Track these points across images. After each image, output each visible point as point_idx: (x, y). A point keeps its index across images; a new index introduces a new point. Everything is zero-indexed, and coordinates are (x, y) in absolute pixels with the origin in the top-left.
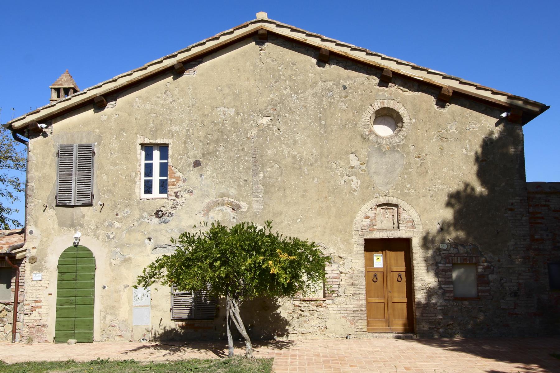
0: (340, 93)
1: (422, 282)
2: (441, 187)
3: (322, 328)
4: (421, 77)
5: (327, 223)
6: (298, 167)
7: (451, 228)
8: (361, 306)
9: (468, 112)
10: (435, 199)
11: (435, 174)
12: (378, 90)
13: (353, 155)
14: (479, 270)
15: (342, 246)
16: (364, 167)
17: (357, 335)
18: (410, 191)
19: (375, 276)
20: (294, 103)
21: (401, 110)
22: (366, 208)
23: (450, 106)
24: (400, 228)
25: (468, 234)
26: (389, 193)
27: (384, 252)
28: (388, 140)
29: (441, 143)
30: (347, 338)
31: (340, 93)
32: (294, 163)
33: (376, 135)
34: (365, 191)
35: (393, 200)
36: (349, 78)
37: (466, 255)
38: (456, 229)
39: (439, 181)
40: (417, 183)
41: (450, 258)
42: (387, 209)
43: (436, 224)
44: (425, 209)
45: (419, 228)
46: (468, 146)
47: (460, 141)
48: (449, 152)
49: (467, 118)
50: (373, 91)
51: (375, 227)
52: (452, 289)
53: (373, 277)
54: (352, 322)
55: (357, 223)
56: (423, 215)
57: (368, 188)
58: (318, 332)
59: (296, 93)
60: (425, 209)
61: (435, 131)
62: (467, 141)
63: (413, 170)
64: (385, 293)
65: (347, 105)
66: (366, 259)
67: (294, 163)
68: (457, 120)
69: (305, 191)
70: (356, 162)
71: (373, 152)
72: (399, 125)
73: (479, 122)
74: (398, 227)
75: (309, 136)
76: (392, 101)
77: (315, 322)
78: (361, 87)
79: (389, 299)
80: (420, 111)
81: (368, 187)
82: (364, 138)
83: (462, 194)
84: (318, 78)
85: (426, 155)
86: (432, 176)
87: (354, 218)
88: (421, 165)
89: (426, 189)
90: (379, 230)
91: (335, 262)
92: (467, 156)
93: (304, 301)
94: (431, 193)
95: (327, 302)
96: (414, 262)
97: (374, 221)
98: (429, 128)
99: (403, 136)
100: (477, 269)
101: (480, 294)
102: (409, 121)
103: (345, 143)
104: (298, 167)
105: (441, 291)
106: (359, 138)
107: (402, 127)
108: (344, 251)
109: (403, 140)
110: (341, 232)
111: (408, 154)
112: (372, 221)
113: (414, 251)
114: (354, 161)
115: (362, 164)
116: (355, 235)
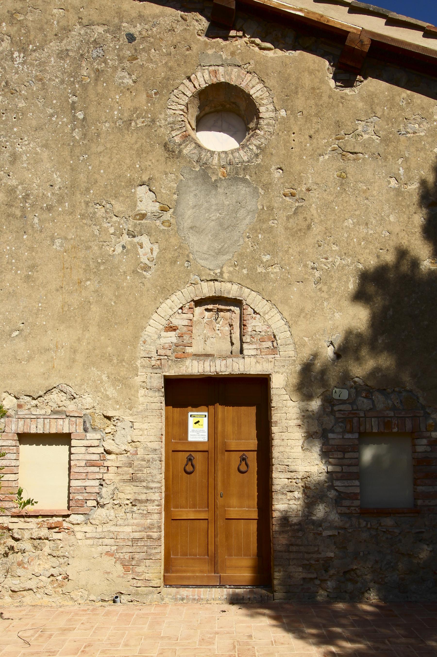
0: (120, 49)
1: (289, 475)
2: (338, 261)
3: (60, 578)
4: (301, 10)
5: (79, 340)
6: (18, 213)
7: (364, 352)
8: (150, 528)
9: (404, 95)
10: (325, 288)
11: (327, 232)
12: (206, 44)
13: (144, 188)
14: (420, 449)
15: (111, 392)
16: (167, 216)
17: (137, 594)
18: (270, 269)
19: (190, 460)
20: (17, 73)
21: (256, 91)
22: (169, 306)
23: (365, 82)
24: (245, 352)
25: (401, 364)
26: (222, 273)
27: (211, 407)
28: (223, 156)
29: (341, 164)
30: (114, 602)
31: (120, 49)
32: (9, 205)
33: (199, 146)
34: (168, 269)
35: (231, 290)
36: (141, 17)
37: (391, 414)
38: (374, 349)
39: (335, 248)
40: (287, 252)
41: (355, 420)
42: (222, 310)
43: (326, 344)
44: (302, 310)
45: (288, 351)
46: (402, 171)
47: (386, 159)
48: (360, 185)
49: (403, 109)
50: (195, 47)
51: (189, 350)
52: (358, 490)
53: (182, 460)
54: (128, 565)
55: (149, 340)
56: (296, 322)
57: (175, 262)
58: (50, 587)
59: (23, 50)
60: (302, 310)
61: (330, 136)
62: (400, 161)
63: (278, 225)
64: (210, 499)
65: (134, 77)
66: (169, 422)
67: (9, 205)
68: (379, 114)
69: (33, 267)
70: (151, 204)
71: (190, 183)
72: (252, 125)
73: (426, 117)
74: (241, 352)
75: (46, 146)
76: (236, 70)
77: (42, 565)
78: (169, 38)
79: (218, 512)
80: (296, 93)
81: (177, 257)
82: (171, 152)
83: (391, 275)
84: (73, 17)
85: (308, 190)
86: (319, 238)
87: (143, 328)
88: (295, 213)
89: (305, 266)
90: (197, 356)
91: (94, 429)
92: (398, 192)
93: (19, 516)
94: (317, 274)
95: (73, 518)
96: (274, 429)
97: (186, 337)
98: (317, 131)
99: (258, 147)
100: (414, 445)
101: (419, 502)
102: (272, 115)
103: (128, 161)
104: (18, 213)
105: (332, 494)
106: (159, 150)
107: (257, 128)
108: (117, 402)
109: (257, 155)
110: (111, 361)
111: (267, 187)
112: (184, 335)
113: (273, 404)
114: (146, 202)
115: (163, 210)
116: (144, 367)
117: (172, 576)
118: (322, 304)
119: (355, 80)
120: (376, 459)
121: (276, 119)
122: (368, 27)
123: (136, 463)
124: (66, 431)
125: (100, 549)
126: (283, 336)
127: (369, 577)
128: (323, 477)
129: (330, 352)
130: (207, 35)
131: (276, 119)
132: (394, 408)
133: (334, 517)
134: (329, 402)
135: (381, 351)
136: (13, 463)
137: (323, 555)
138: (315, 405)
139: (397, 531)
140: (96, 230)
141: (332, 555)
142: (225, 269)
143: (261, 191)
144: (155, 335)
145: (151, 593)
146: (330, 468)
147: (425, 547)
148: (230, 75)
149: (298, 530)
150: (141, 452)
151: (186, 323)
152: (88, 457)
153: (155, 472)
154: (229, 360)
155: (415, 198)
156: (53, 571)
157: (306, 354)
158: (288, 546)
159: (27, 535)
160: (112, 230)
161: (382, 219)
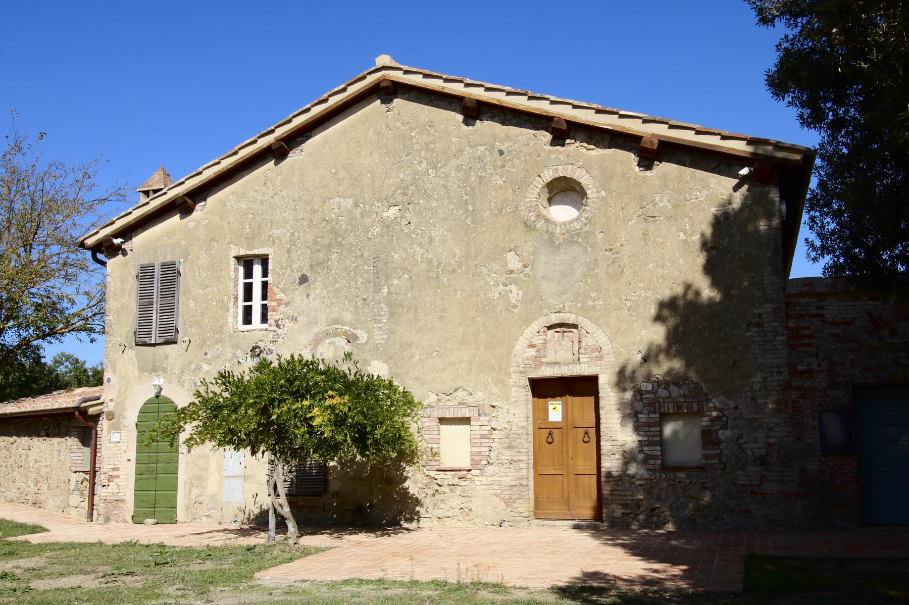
0: (495, 161)
5: (474, 356)
6: (434, 276)
7: (662, 357)
8: (521, 478)
10: (634, 314)
12: (550, 151)
15: (495, 390)
17: (514, 521)
18: (596, 302)
25: (688, 365)
26: (564, 307)
31: (495, 161)
33: (547, 221)
35: (571, 318)
39: (641, 285)
40: (608, 290)
41: (657, 404)
43: (636, 353)
44: (619, 329)
46: (688, 227)
47: (676, 219)
48: (658, 239)
49: (687, 182)
50: (542, 154)
51: (544, 360)
53: (546, 434)
54: (508, 502)
60: (619, 329)
65: (504, 179)
69: (444, 310)
73: (706, 186)
75: (450, 230)
76: (570, 167)
77: (455, 502)
80: (612, 179)
82: (529, 227)
83: (681, 302)
85: (622, 245)
87: (514, 347)
88: (613, 262)
89: (621, 299)
92: (685, 242)
94: (629, 304)
97: (542, 352)
98: (627, 204)
99: (586, 219)
102: (596, 195)
104: (434, 276)
105: (641, 456)
106: (521, 226)
108: (498, 396)
109: (586, 224)
114: (513, 262)
115: (525, 266)
117: (540, 511)
118: (633, 325)
119: (653, 164)
120: (675, 433)
121: (598, 198)
122: (656, 132)
123: (511, 436)
124: (467, 416)
125: (490, 492)
126: (607, 347)
127: (668, 513)
128: (635, 445)
129: (638, 358)
130: (551, 145)
131: (598, 198)
132: (684, 396)
133: (642, 472)
134: (639, 393)
135: (675, 356)
136: (436, 437)
137: (635, 497)
138: (628, 395)
139: (688, 481)
140: (482, 283)
141: (642, 497)
142: (566, 304)
143: (589, 249)
144: (522, 351)
145: (523, 521)
146: (640, 438)
147: (709, 493)
148: (566, 171)
149: (619, 480)
150: (514, 428)
151: (541, 342)
152: (482, 432)
153: (523, 442)
154: (570, 366)
155: (698, 245)
156: (462, 506)
157: (621, 360)
158: (612, 491)
159: (446, 483)
160: (492, 283)
161: (674, 262)
